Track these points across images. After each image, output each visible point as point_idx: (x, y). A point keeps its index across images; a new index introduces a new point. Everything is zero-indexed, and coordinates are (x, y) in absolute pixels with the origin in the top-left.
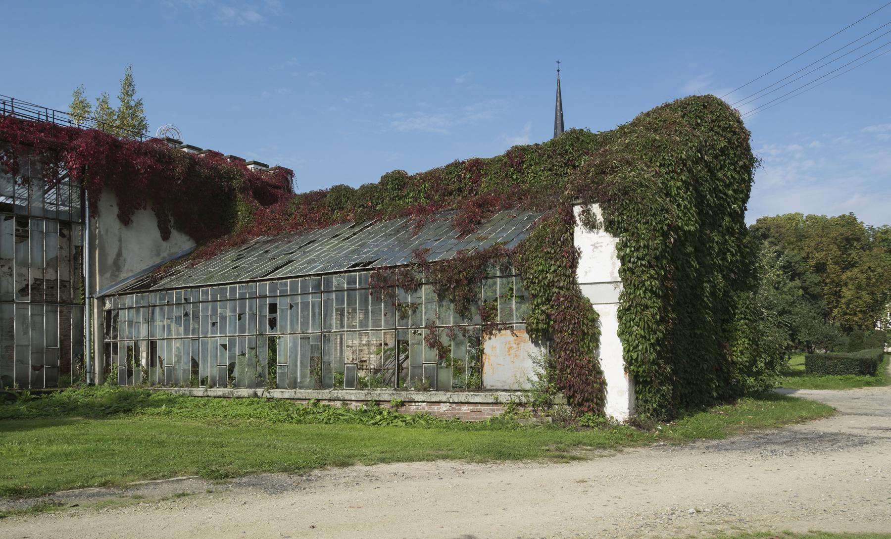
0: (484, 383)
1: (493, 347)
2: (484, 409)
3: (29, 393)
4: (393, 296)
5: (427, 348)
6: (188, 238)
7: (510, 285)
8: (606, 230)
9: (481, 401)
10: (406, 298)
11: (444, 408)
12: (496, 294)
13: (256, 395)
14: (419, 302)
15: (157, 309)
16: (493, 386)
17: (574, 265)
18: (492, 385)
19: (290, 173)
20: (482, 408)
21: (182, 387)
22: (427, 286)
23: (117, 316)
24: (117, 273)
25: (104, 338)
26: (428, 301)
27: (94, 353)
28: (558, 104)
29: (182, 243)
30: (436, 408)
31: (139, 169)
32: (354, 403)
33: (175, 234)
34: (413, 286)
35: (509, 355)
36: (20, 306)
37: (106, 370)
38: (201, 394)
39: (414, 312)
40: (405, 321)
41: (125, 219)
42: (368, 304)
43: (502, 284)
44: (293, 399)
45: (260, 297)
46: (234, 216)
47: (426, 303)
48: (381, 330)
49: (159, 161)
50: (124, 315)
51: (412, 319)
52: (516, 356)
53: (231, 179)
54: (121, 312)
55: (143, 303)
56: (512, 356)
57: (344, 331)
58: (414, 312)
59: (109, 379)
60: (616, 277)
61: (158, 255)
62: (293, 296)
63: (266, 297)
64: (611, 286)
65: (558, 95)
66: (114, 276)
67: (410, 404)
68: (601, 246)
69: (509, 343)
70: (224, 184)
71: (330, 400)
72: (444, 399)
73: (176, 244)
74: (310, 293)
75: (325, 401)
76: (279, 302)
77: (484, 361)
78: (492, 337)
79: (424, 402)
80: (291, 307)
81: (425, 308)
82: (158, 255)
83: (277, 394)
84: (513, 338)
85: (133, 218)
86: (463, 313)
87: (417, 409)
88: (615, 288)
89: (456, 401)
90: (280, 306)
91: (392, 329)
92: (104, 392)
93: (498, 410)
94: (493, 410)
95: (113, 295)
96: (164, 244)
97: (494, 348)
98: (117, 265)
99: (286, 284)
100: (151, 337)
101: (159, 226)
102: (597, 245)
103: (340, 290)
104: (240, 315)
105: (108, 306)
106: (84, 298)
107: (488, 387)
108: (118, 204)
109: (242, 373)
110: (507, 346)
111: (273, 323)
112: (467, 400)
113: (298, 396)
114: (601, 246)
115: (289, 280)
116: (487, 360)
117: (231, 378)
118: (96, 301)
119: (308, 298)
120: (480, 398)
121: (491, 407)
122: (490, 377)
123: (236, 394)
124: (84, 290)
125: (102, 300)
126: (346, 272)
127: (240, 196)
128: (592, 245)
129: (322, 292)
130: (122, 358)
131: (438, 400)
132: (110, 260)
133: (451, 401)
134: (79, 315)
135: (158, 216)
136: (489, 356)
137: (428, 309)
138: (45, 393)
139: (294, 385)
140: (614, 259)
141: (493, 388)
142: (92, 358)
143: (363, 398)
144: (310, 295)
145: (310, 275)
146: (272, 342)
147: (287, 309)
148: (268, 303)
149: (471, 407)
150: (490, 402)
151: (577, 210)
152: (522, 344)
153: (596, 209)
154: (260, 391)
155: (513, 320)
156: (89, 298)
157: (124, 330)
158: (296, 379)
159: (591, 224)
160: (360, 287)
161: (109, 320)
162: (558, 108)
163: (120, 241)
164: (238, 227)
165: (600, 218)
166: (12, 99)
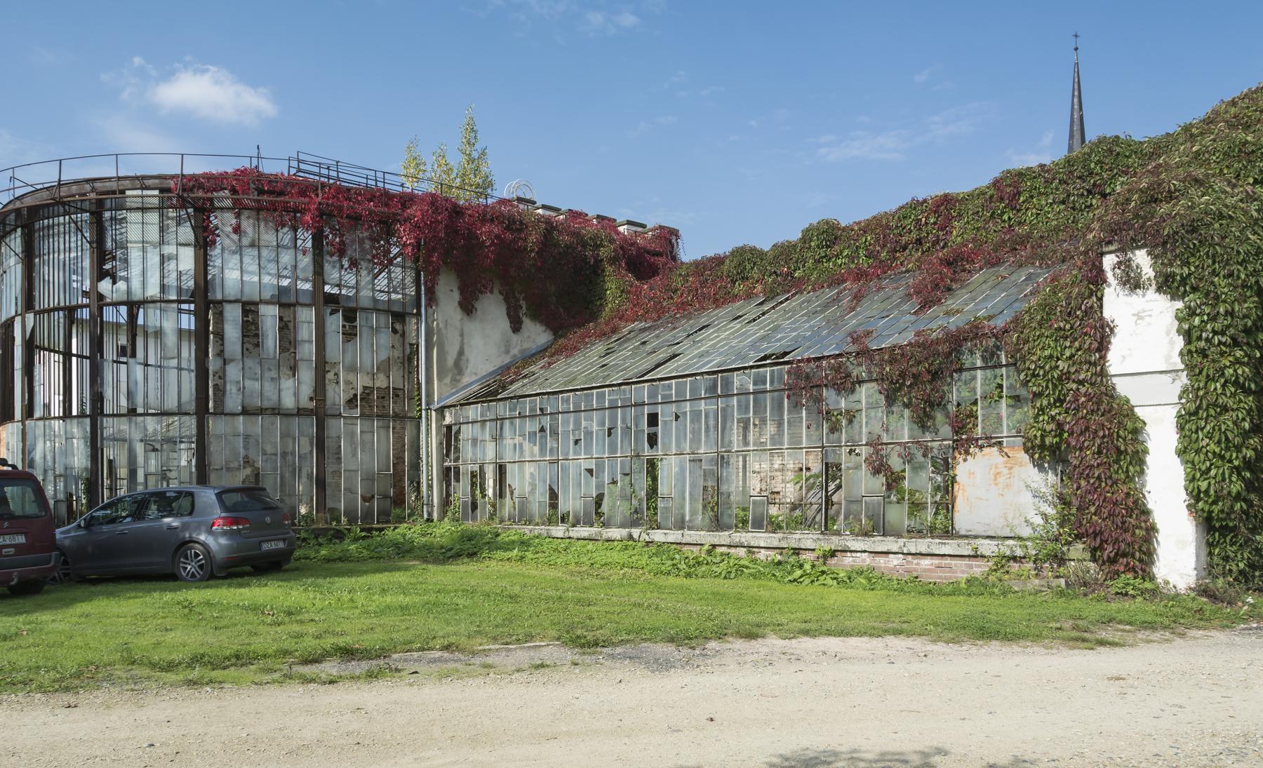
3: (359, 530)
6: (543, 328)
10: (838, 403)
11: (895, 561)
12: (975, 394)
13: (631, 537)
15: (507, 423)
17: (1103, 346)
19: (674, 233)
20: (953, 562)
21: (537, 524)
23: (458, 432)
24: (458, 378)
25: (444, 461)
26: (871, 407)
27: (432, 480)
28: (1076, 100)
29: (536, 335)
31: (484, 242)
33: (527, 323)
34: (846, 384)
35: (996, 484)
37: (446, 502)
38: (560, 534)
39: (850, 422)
40: (836, 435)
41: (468, 307)
43: (985, 379)
44: (680, 543)
46: (602, 296)
47: (867, 409)
49: (508, 228)
50: (467, 432)
51: (846, 431)
52: (1007, 486)
53: (597, 247)
54: (463, 427)
55: (490, 415)
58: (850, 422)
59: (449, 514)
65: (1076, 87)
66: (455, 381)
67: (844, 554)
68: (1150, 316)
69: (996, 467)
73: (529, 337)
74: (702, 398)
77: (956, 493)
78: (969, 457)
79: (865, 551)
80: (677, 417)
81: (866, 416)
82: (507, 352)
83: (658, 536)
85: (478, 305)
86: (923, 421)
88: (1174, 380)
92: (444, 531)
93: (979, 566)
95: (454, 406)
96: (515, 338)
97: (971, 474)
98: (459, 367)
99: (670, 387)
101: (508, 315)
104: (610, 430)
105: (448, 420)
106: (420, 410)
107: (963, 532)
108: (459, 288)
109: (612, 507)
110: (993, 471)
112: (929, 551)
113: (687, 539)
114: (1150, 316)
115: (673, 381)
116: (961, 492)
118: (434, 413)
120: (950, 547)
122: (964, 518)
123: (605, 536)
124: (420, 400)
125: (441, 411)
127: (609, 269)
128: (1134, 315)
132: (450, 361)
134: (415, 432)
135: (506, 300)
136: (964, 486)
137: (870, 418)
138: (377, 530)
139: (681, 525)
141: (970, 533)
142: (430, 487)
143: (775, 544)
144: (703, 401)
145: (702, 374)
146: (652, 466)
148: (646, 412)
149: (936, 561)
150: (966, 553)
152: (1016, 469)
153: (1142, 259)
154: (636, 532)
155: (1002, 432)
156: (427, 410)
157: (467, 451)
158: (683, 517)
159: (1132, 283)
160: (772, 388)
161: (450, 437)
162: (1076, 107)
163: (462, 335)
166: (337, 162)
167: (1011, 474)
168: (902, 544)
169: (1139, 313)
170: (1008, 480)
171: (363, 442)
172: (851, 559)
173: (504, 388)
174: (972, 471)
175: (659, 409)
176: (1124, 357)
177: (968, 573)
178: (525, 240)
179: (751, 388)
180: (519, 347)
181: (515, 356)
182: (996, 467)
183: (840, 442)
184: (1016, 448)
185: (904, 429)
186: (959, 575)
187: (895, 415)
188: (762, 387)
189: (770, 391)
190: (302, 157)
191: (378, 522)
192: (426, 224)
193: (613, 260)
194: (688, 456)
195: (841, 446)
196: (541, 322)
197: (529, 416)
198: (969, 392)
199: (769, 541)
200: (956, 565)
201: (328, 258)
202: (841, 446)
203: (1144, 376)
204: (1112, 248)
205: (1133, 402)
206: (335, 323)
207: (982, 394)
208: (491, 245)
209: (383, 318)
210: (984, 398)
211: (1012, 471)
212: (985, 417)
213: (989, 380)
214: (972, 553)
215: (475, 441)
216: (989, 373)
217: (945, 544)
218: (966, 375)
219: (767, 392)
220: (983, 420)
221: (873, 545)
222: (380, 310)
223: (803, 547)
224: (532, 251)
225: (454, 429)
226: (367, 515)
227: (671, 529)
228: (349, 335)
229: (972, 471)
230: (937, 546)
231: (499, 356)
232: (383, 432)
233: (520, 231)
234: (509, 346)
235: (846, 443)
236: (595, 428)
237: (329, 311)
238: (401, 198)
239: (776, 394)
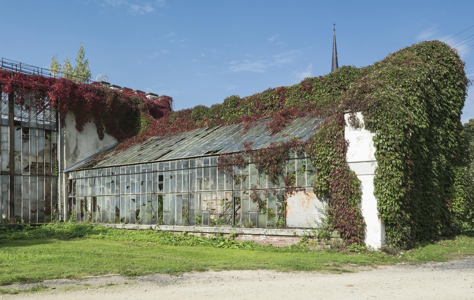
3: (29, 225)
4: (231, 171)
6: (113, 138)
10: (239, 172)
11: (262, 238)
12: (295, 169)
13: (151, 228)
15: (97, 179)
17: (344, 151)
18: (292, 224)
19: (170, 99)
20: (286, 239)
21: (110, 223)
22: (252, 165)
23: (75, 183)
24: (75, 159)
25: (68, 195)
26: (253, 174)
27: (63, 203)
28: (334, 51)
29: (110, 141)
31: (87, 100)
32: (208, 234)
33: (106, 136)
34: (243, 164)
35: (303, 206)
36: (25, 177)
38: (120, 227)
40: (238, 185)
41: (80, 128)
44: (173, 231)
45: (154, 172)
46: (139, 125)
47: (251, 175)
49: (98, 95)
50: (79, 182)
51: (242, 184)
53: (137, 104)
54: (77, 181)
55: (89, 175)
58: (244, 180)
59: (71, 218)
60: (373, 158)
61: (97, 148)
63: (157, 171)
65: (334, 45)
66: (74, 160)
67: (241, 235)
68: (363, 139)
69: (303, 199)
70: (133, 107)
71: (194, 232)
72: (262, 233)
77: (287, 210)
78: (292, 195)
79: (250, 234)
81: (251, 178)
82: (97, 148)
83: (163, 228)
84: (305, 196)
85: (84, 127)
86: (274, 180)
92: (68, 226)
93: (296, 240)
95: (73, 171)
96: (101, 142)
98: (75, 154)
99: (168, 164)
101: (98, 132)
102: (360, 138)
104: (142, 182)
105: (71, 177)
106: (58, 173)
107: (290, 226)
110: (302, 201)
111: (161, 187)
114: (363, 139)
115: (170, 162)
117: (138, 219)
118: (64, 174)
123: (140, 228)
125: (67, 173)
126: (203, 157)
127: (142, 113)
128: (356, 138)
129: (189, 168)
130: (78, 206)
132: (72, 152)
134: (55, 182)
135: (97, 126)
136: (290, 207)
137: (252, 178)
138: (38, 225)
139: (173, 223)
140: (371, 147)
142: (62, 206)
143: (213, 231)
144: (182, 170)
145: (182, 159)
146: (161, 198)
148: (158, 175)
152: (311, 200)
153: (359, 116)
154: (153, 226)
155: (305, 185)
156: (61, 173)
157: (79, 191)
158: (174, 219)
159: (356, 125)
160: (211, 166)
161: (71, 185)
162: (334, 53)
163: (77, 140)
164: (141, 132)
166: (20, 63)
168: (265, 231)
171: (32, 187)
172: (244, 237)
173: (96, 164)
175: (164, 174)
176: (353, 155)
178: (105, 100)
179: (203, 165)
180: (102, 146)
181: (101, 150)
182: (303, 199)
185: (266, 183)
190: (4, 60)
191: (38, 222)
192: (61, 91)
193: (144, 110)
196: (112, 135)
197: (107, 176)
201: (16, 105)
204: (348, 111)
205: (356, 173)
206: (19, 134)
208: (90, 102)
209: (41, 132)
211: (310, 201)
212: (299, 179)
215: (82, 187)
216: (300, 160)
222: (39, 129)
224: (108, 105)
225: (73, 181)
226: (33, 219)
228: (26, 139)
231: (94, 150)
232: (41, 182)
233: (103, 96)
234: (98, 145)
236: (136, 181)
237: (16, 128)
238: (49, 80)
239: (213, 168)
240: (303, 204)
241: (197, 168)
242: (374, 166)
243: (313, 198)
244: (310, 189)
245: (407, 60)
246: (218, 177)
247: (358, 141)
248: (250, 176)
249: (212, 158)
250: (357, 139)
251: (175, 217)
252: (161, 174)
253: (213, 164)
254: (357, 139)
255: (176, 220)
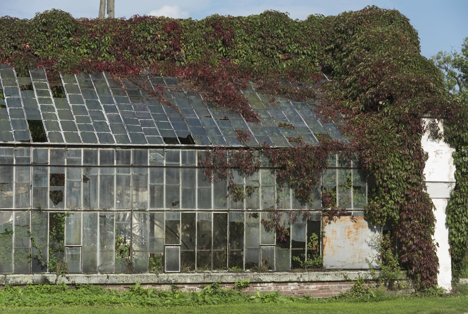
0: (324, 264)
1: (333, 231)
2: (332, 287)
5: (264, 231)
7: (348, 176)
8: (445, 141)
9: (331, 280)
10: (240, 181)
11: (292, 287)
12: (335, 183)
13: (45, 281)
14: (256, 184)
16: (333, 266)
17: (422, 166)
18: (332, 265)
20: (330, 285)
22: (264, 171)
26: (266, 186)
30: (283, 288)
32: (186, 286)
35: (349, 238)
39: (250, 195)
40: (239, 203)
42: (195, 184)
43: (340, 175)
47: (263, 187)
48: (212, 211)
51: (247, 201)
52: (355, 239)
56: (352, 239)
57: (163, 211)
58: (250, 195)
60: (452, 179)
62: (104, 168)
64: (446, 185)
67: (254, 285)
68: (442, 153)
69: (349, 228)
72: (294, 279)
74: (114, 167)
75: (148, 286)
76: (68, 173)
77: (324, 243)
78: (332, 222)
81: (262, 191)
84: (352, 224)
87: (262, 289)
88: (449, 186)
89: (307, 279)
90: (68, 177)
91: (231, 211)
93: (346, 287)
94: (341, 287)
99: (78, 153)
100: (11, 205)
102: (439, 152)
103: (156, 166)
107: (328, 267)
110: (347, 230)
112: (318, 279)
114: (442, 153)
115: (82, 149)
116: (327, 243)
119: (97, 172)
120: (322, 276)
121: (338, 285)
128: (435, 152)
131: (287, 279)
133: (301, 280)
136: (329, 239)
137: (265, 193)
140: (450, 164)
141: (332, 268)
143: (201, 280)
144: (115, 169)
147: (80, 182)
148: (49, 172)
149: (319, 286)
150: (340, 279)
151: (426, 122)
152: (360, 229)
155: (351, 207)
158: (94, 262)
159: (435, 136)
160: (184, 165)
165: (442, 130)
167: (357, 232)
168: (300, 276)
169: (437, 151)
170: (356, 236)
172: (260, 288)
174: (334, 230)
176: (430, 173)
177: (339, 291)
179: (165, 163)
182: (349, 228)
183: (242, 208)
184: (360, 217)
186: (334, 293)
187: (283, 192)
188: (175, 163)
189: (182, 167)
194: (98, 213)
195: (244, 211)
198: (331, 182)
199: (195, 278)
200: (332, 287)
202: (244, 211)
203: (434, 183)
204: (427, 116)
205: (430, 197)
207: (339, 183)
210: (340, 186)
211: (358, 230)
212: (341, 198)
213: (343, 176)
214: (344, 279)
216: (343, 171)
217: (327, 274)
218: (329, 171)
219: (180, 167)
220: (339, 200)
221: (279, 278)
223: (224, 281)
227: (81, 273)
229: (334, 230)
230: (313, 276)
235: (247, 209)
239: (188, 169)
240: (348, 235)
241: (150, 167)
242: (450, 188)
243: (363, 227)
244: (358, 213)
245: (177, 21)
246: (199, 185)
247: (437, 155)
248: (260, 190)
249: (185, 152)
250: (435, 153)
251: (95, 256)
252: (57, 171)
253: (188, 163)
254: (435, 153)
255: (98, 264)
